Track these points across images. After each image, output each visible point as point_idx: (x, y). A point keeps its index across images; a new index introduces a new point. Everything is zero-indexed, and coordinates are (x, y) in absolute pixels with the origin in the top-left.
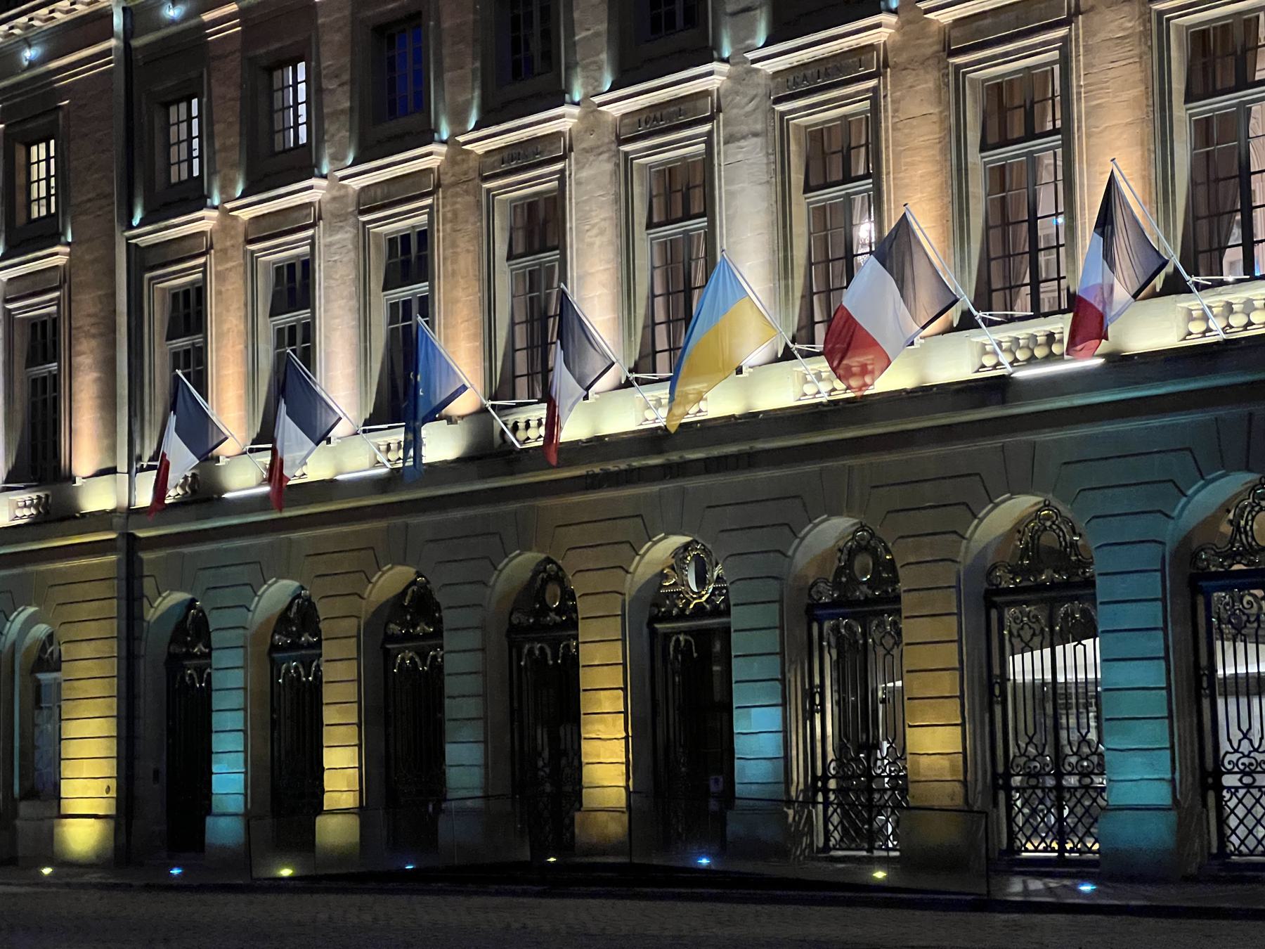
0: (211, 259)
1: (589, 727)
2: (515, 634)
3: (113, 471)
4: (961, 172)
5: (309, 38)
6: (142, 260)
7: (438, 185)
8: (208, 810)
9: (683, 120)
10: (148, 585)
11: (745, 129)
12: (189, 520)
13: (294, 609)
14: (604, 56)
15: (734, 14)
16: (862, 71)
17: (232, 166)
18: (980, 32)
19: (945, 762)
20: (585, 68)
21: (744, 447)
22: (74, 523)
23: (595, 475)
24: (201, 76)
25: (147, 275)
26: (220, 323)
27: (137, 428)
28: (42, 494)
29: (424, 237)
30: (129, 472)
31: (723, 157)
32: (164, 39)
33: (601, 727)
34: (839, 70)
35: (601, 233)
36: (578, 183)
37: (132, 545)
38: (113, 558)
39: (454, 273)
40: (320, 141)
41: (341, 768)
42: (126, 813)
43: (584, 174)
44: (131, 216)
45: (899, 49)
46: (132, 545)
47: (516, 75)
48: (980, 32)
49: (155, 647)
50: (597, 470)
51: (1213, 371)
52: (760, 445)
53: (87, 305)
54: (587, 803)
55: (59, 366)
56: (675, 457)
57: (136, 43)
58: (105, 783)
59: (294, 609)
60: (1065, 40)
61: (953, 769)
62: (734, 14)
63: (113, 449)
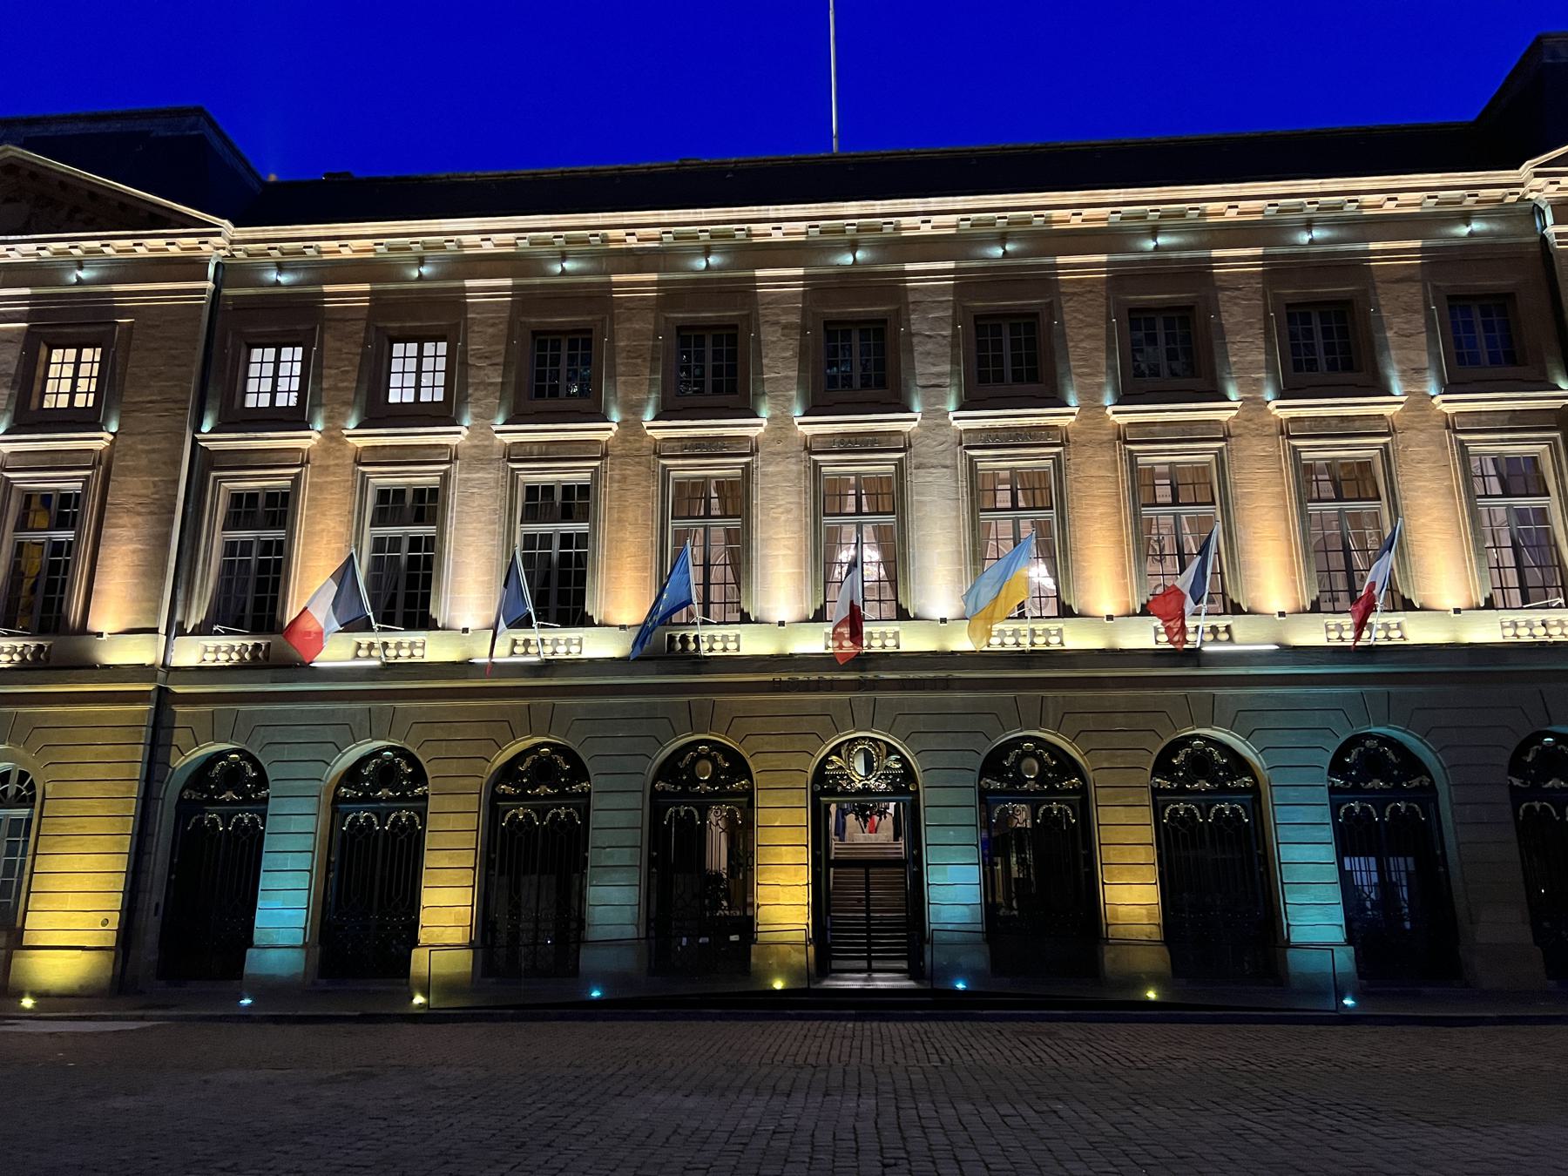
0: (307, 472)
1: (767, 875)
2: (658, 803)
3: (155, 631)
4: (510, 533)
5: (458, 324)
6: (205, 462)
7: (605, 455)
8: (249, 943)
9: (877, 447)
10: (179, 737)
11: (935, 462)
12: (659, 673)
13: (528, 761)
14: (794, 393)
15: (924, 387)
16: (1050, 441)
17: (345, 403)
18: (1015, 438)
19: (1143, 911)
20: (772, 398)
21: (942, 674)
22: (95, 672)
23: (867, 680)
24: (314, 329)
25: (214, 474)
26: (311, 521)
27: (180, 596)
28: (262, 642)
29: (584, 490)
30: (167, 634)
31: (917, 480)
32: (266, 295)
33: (782, 876)
34: (710, 446)
35: (788, 511)
36: (765, 475)
37: (164, 698)
38: (147, 707)
39: (620, 520)
40: (463, 400)
41: (447, 909)
42: (488, 931)
43: (771, 469)
44: (200, 423)
45: (1078, 433)
46: (164, 698)
47: (540, 393)
48: (1153, 434)
49: (171, 792)
50: (784, 678)
51: (1371, 663)
52: (957, 675)
53: (130, 489)
54: (761, 937)
55: (78, 536)
56: (870, 676)
57: (226, 292)
58: (100, 917)
59: (528, 761)
60: (298, 476)
61: (1150, 915)
62: (924, 387)
63: (156, 612)
